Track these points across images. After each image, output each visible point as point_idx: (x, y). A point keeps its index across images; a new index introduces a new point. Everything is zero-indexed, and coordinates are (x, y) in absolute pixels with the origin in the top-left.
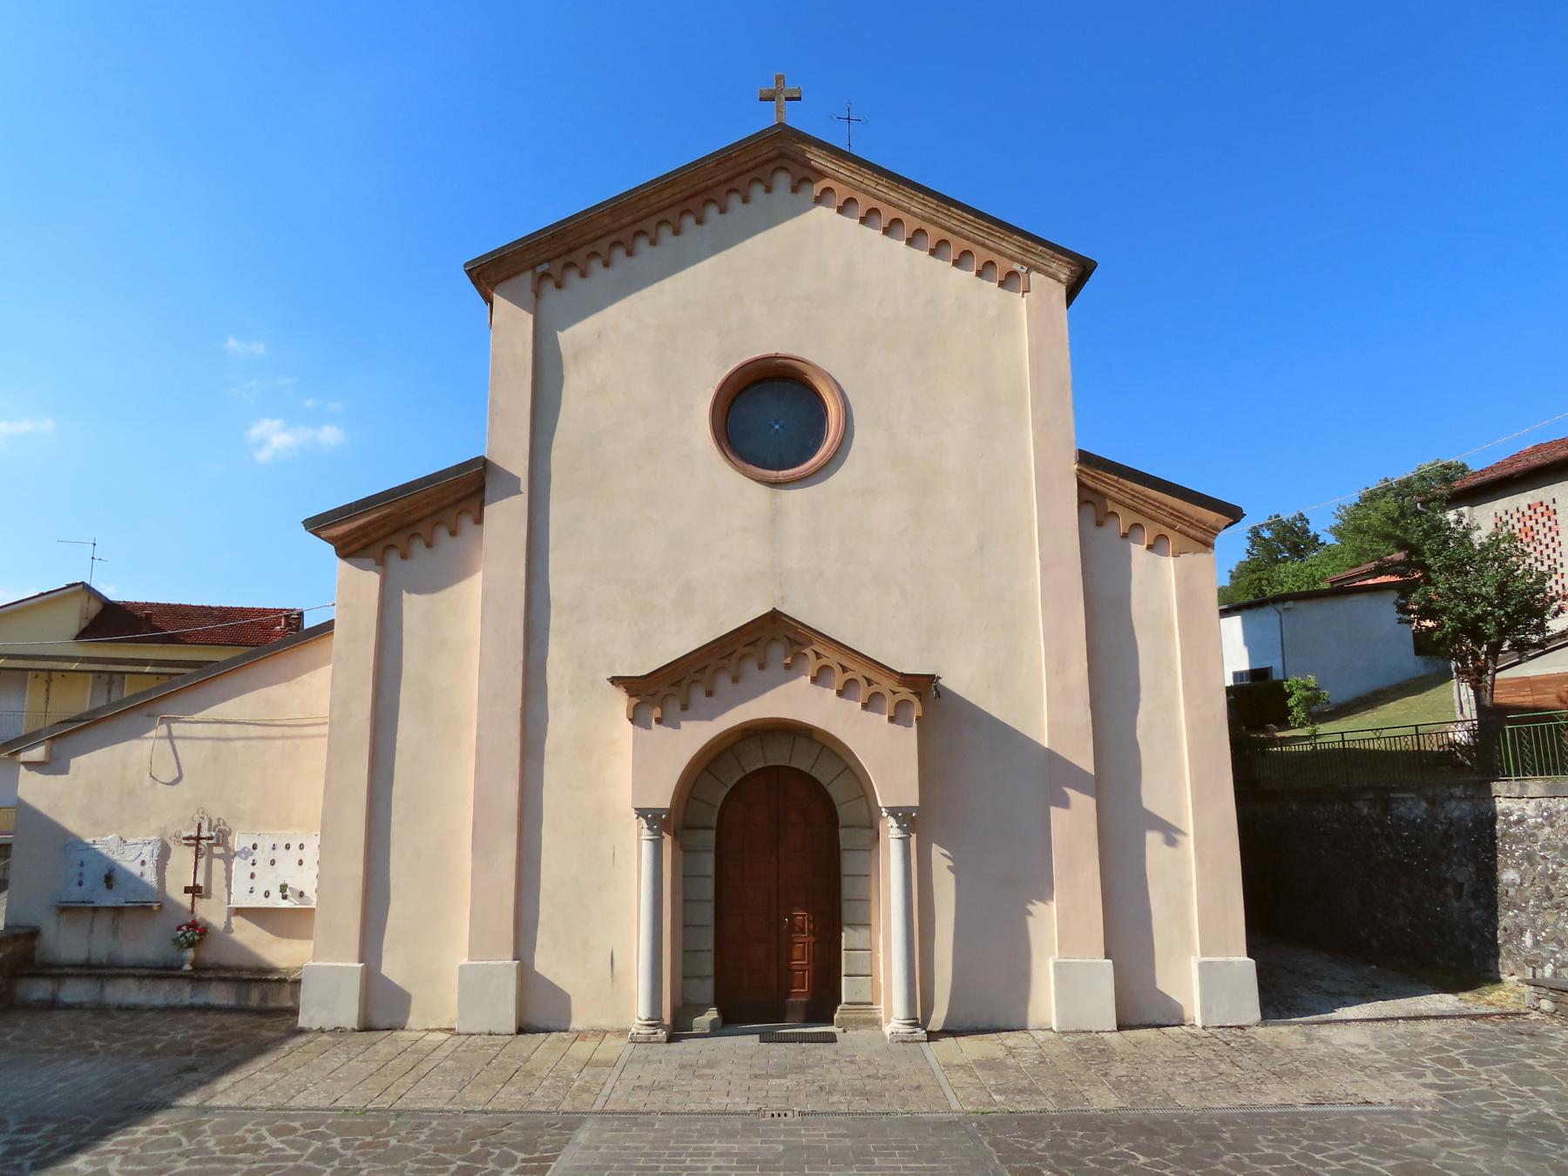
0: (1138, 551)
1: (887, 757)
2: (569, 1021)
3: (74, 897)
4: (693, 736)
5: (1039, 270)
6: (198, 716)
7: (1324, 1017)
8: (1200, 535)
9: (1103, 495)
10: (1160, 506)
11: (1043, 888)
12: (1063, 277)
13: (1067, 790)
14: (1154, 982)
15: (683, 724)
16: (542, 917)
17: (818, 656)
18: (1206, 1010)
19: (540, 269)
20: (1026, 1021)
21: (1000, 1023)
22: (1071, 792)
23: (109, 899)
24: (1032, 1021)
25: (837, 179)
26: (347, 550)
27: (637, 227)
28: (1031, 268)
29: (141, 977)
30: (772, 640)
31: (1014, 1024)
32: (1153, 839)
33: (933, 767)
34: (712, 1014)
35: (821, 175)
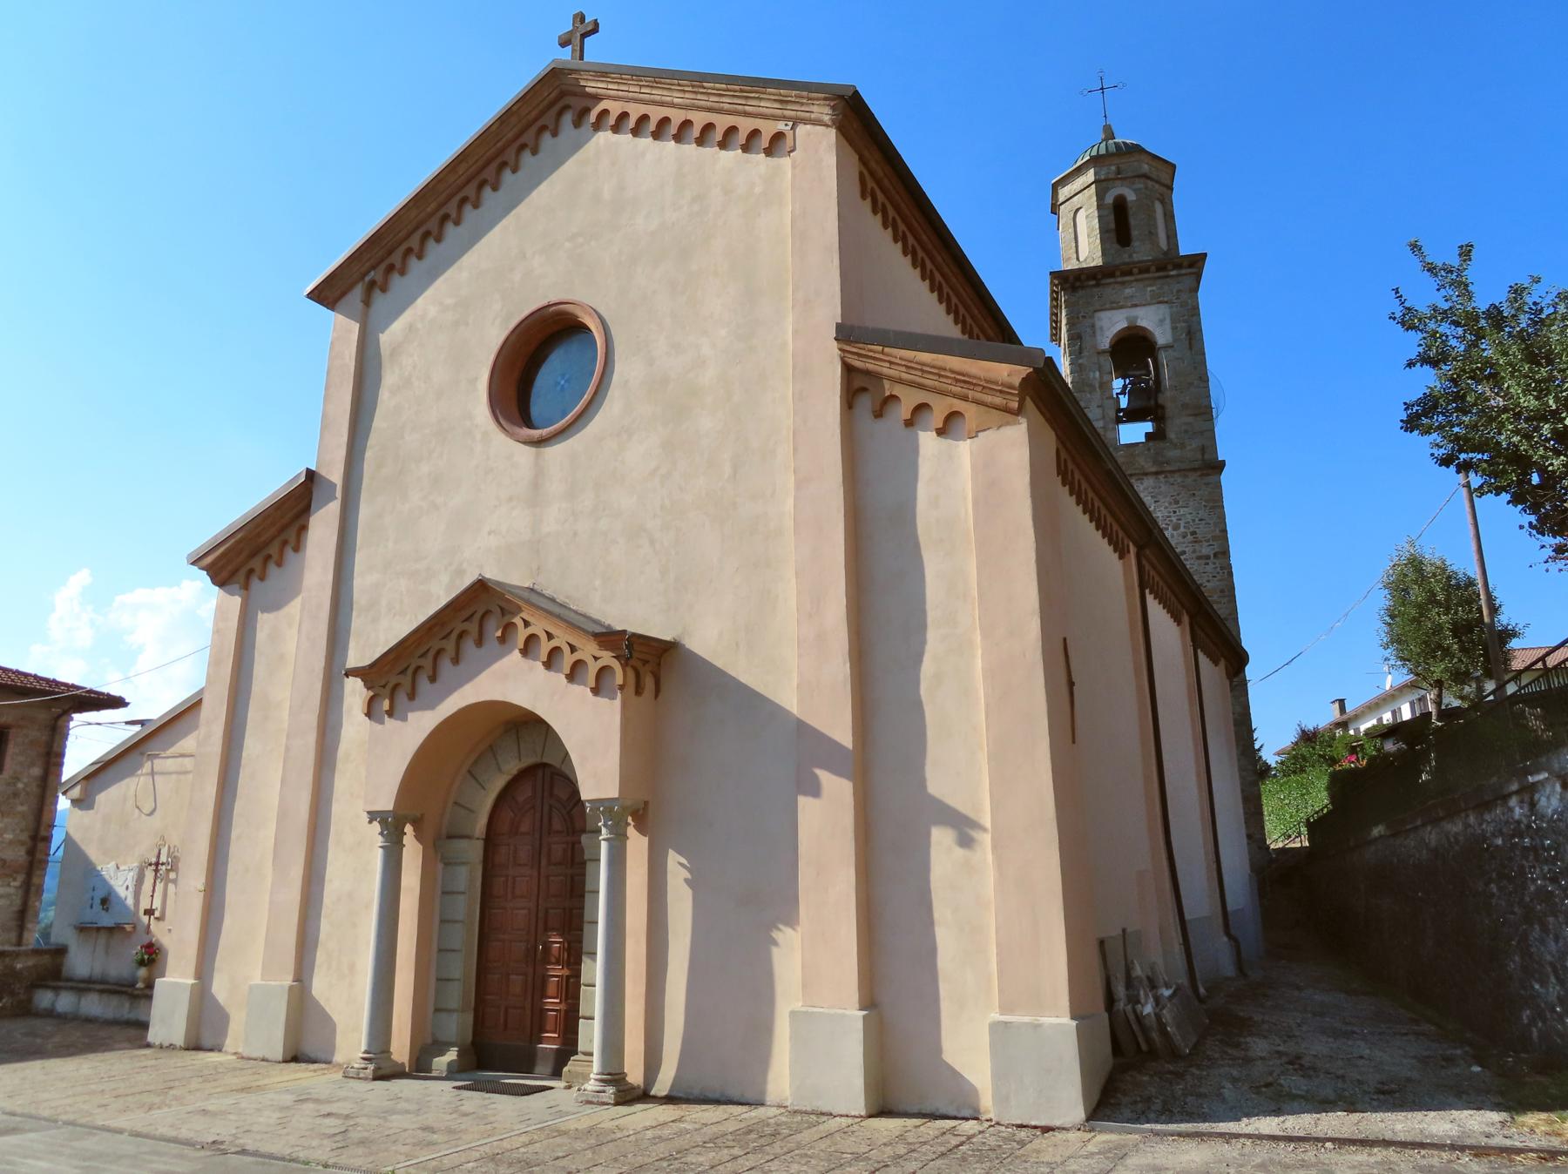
0: (928, 440)
1: (594, 737)
2: (333, 1054)
3: (87, 919)
4: (419, 725)
5: (805, 121)
6: (170, 752)
7: (1204, 1127)
8: (998, 400)
9: (877, 377)
10: (939, 372)
11: (787, 911)
12: (827, 118)
13: (819, 772)
14: (938, 1049)
15: (410, 715)
16: (322, 936)
17: (527, 624)
18: (1001, 1099)
19: (367, 279)
20: (763, 1092)
21: (734, 1093)
22: (824, 776)
23: (106, 920)
24: (771, 1097)
25: (609, 97)
26: (225, 574)
27: (441, 213)
28: (796, 122)
29: (102, 992)
30: (478, 616)
31: (749, 1096)
32: (941, 839)
33: (645, 749)
34: (452, 1055)
35: (597, 98)
